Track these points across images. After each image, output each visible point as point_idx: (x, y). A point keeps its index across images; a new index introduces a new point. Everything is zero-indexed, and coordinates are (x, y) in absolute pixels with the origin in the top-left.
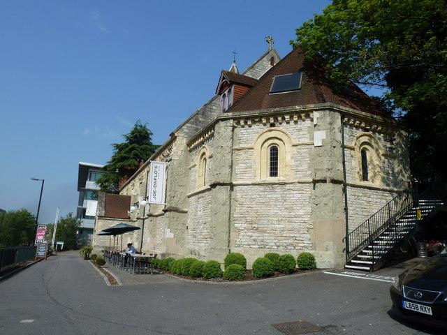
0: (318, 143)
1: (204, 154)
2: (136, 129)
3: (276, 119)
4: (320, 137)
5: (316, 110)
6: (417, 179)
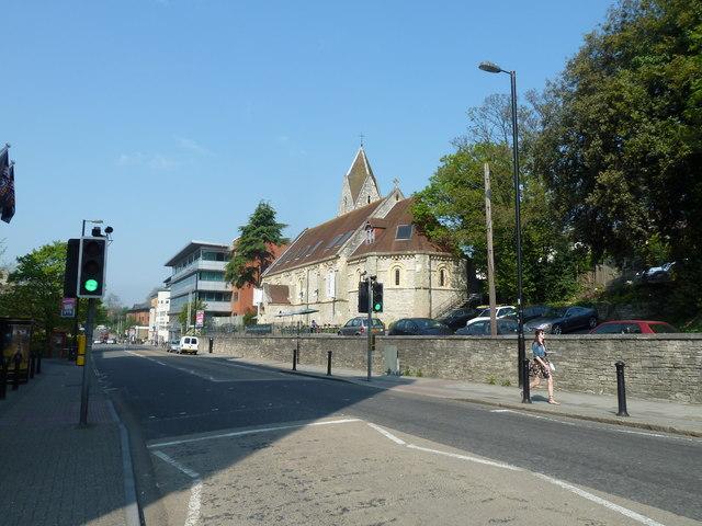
0: (418, 270)
2: (260, 209)
4: (419, 267)
6: (556, 257)
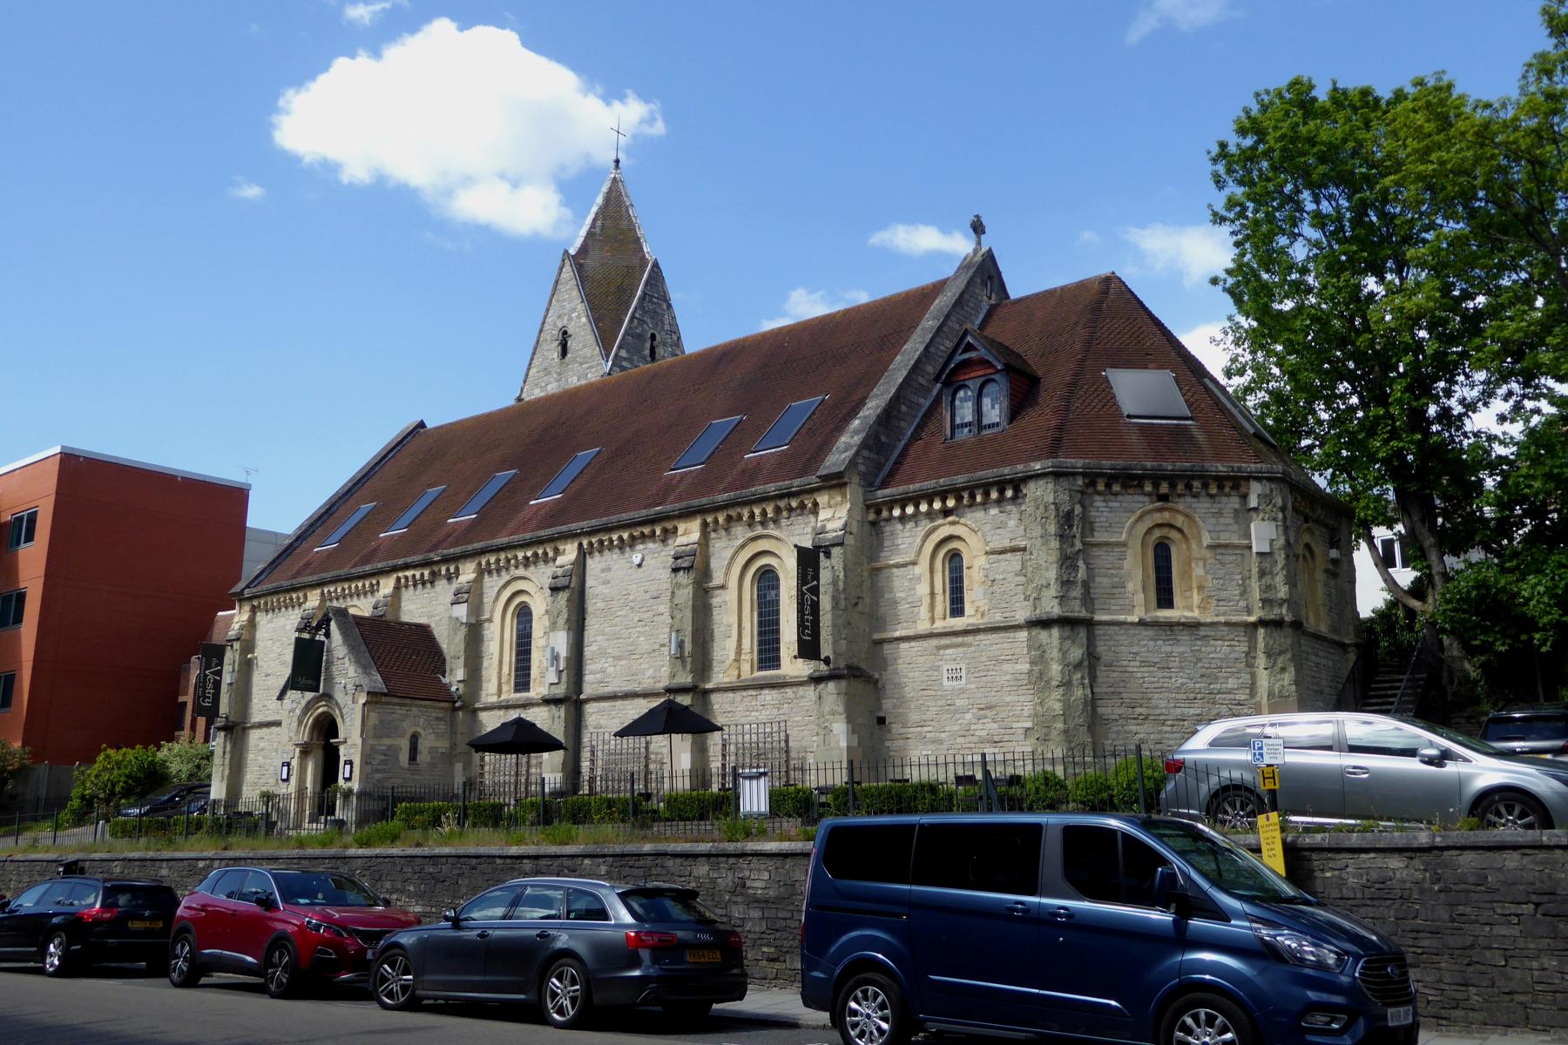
1: (603, 571)
3: (1173, 486)
5: (1258, 479)
